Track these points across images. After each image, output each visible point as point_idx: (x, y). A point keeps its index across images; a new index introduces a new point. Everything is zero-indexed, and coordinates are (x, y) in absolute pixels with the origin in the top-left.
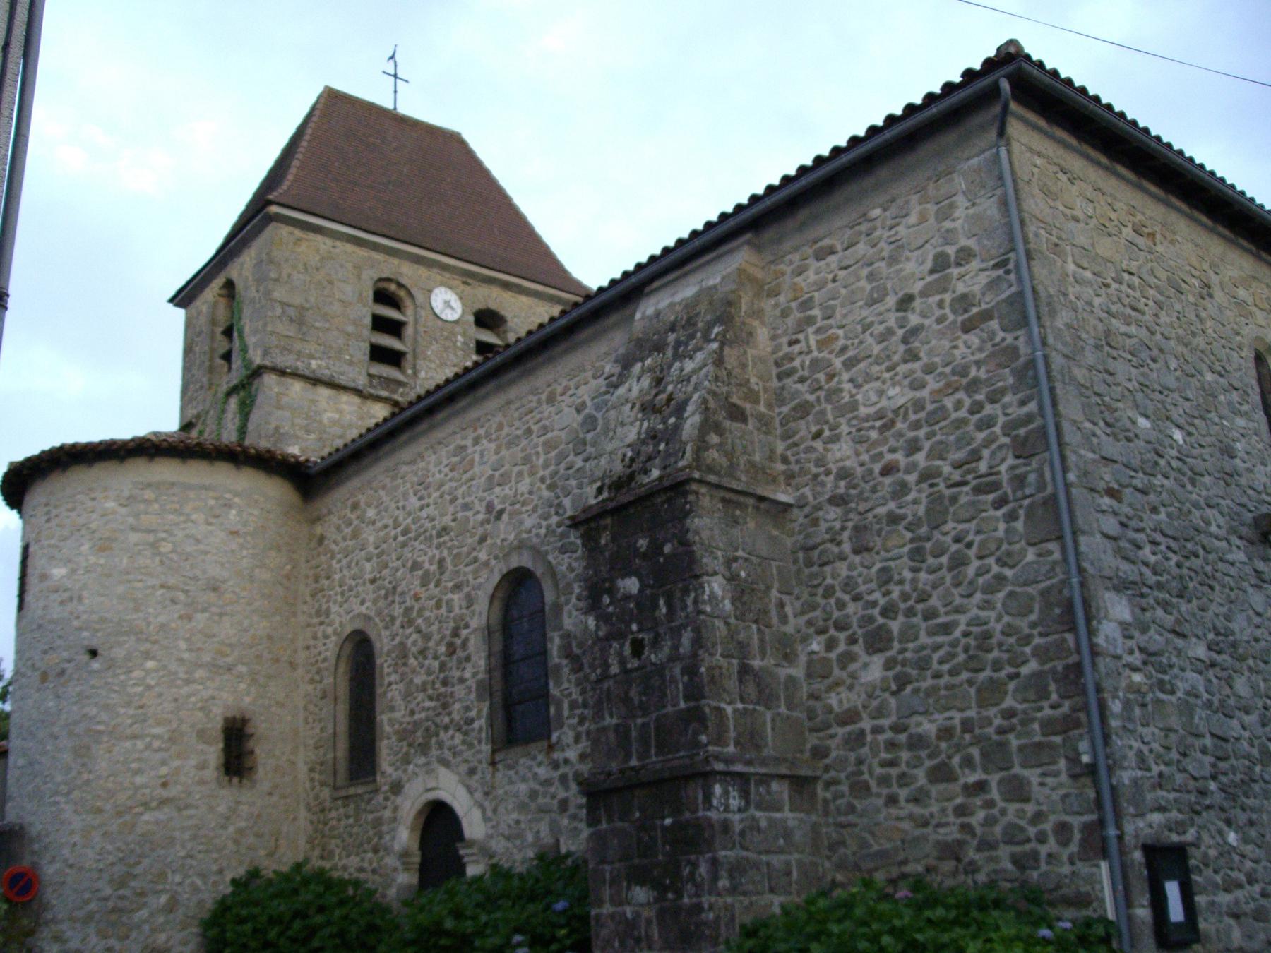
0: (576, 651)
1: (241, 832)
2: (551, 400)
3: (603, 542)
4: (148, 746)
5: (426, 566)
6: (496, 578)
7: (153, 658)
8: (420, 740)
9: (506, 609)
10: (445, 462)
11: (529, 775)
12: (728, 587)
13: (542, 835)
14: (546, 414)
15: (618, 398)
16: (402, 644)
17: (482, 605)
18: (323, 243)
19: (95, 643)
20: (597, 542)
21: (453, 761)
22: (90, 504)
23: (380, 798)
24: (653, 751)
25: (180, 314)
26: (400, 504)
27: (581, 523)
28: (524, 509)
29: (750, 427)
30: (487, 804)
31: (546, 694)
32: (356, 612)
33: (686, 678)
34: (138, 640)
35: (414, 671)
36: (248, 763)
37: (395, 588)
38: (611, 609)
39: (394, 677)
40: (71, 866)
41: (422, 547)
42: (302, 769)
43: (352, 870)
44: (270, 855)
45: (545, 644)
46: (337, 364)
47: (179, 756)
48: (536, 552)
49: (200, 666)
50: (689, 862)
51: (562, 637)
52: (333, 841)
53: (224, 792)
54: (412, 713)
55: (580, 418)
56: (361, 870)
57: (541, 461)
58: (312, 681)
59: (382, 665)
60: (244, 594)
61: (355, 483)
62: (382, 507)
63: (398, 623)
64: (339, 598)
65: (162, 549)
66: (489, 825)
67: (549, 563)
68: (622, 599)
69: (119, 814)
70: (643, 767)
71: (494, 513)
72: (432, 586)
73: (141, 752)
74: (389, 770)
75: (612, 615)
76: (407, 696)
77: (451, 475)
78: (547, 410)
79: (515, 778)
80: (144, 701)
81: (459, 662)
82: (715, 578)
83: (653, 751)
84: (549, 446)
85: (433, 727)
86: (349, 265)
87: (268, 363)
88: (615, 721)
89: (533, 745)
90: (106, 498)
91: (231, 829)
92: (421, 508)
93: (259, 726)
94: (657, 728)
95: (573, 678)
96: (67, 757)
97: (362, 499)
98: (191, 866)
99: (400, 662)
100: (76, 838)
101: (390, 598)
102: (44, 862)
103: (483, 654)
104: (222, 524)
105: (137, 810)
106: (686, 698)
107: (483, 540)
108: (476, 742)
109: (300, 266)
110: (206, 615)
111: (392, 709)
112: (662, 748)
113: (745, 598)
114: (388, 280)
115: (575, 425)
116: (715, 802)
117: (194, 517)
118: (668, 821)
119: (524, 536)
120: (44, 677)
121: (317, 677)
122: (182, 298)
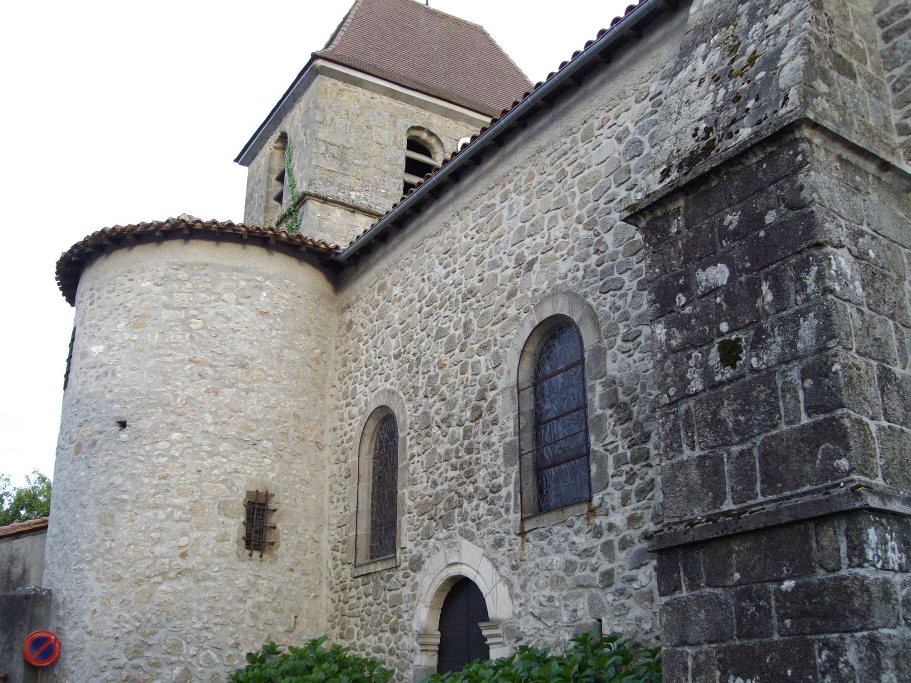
0: (622, 398)
1: (259, 606)
2: (586, 138)
3: (674, 230)
4: (169, 517)
5: (452, 331)
6: (528, 330)
7: (179, 430)
8: (443, 513)
9: (538, 366)
10: (472, 225)
11: (565, 545)
12: (856, 266)
13: (580, 613)
14: (582, 151)
15: (679, 82)
16: (425, 413)
17: (511, 361)
18: (364, 95)
19: (124, 416)
20: (665, 232)
21: (477, 533)
22: (128, 284)
23: (400, 574)
24: (758, 487)
25: (244, 171)
26: (425, 277)
27: (641, 212)
28: (558, 255)
29: (859, 85)
30: (515, 579)
31: (585, 453)
32: (381, 389)
33: (809, 383)
34: (166, 412)
35: (437, 441)
36: (271, 538)
37: (418, 359)
38: (688, 310)
39: (416, 449)
40: (90, 633)
41: (448, 313)
42: (326, 547)
43: (370, 650)
44: (289, 631)
45: (585, 397)
46: (374, 196)
47: (199, 528)
48: (572, 295)
49: (225, 439)
50: (826, 644)
51: (604, 385)
52: (352, 620)
53: (244, 565)
54: (435, 484)
55: (622, 147)
56: (379, 650)
57: (577, 200)
58: (338, 461)
59: (405, 438)
60: (273, 372)
61: (383, 264)
62: (407, 283)
63: (421, 393)
64: (365, 378)
65: (192, 326)
66: (516, 603)
67: (590, 306)
68: (704, 296)
69: (138, 583)
70: (743, 511)
71: (524, 265)
72: (457, 351)
73: (162, 521)
74: (410, 546)
75: (689, 317)
76: (429, 468)
77: (477, 236)
78: (582, 147)
79: (547, 548)
80: (168, 471)
81: (485, 426)
82: (839, 251)
83: (758, 487)
84: (585, 185)
85: (456, 497)
86: (386, 114)
87: (311, 191)
88: (698, 452)
89: (570, 510)
90: (143, 278)
91: (250, 603)
92: (447, 276)
93: (282, 502)
94: (764, 456)
95: (619, 429)
96: (93, 525)
97: (389, 280)
98: (207, 639)
99: (423, 433)
100: (96, 605)
101: (415, 370)
102: (66, 628)
103: (512, 415)
104: (252, 305)
105: (155, 579)
106: (809, 411)
107: (512, 294)
108: (502, 511)
109: (343, 113)
110: (234, 390)
111: (414, 482)
112: (771, 482)
113: (877, 285)
114: (420, 128)
115: (616, 155)
116: (870, 554)
117: (225, 296)
118: (788, 585)
119: (559, 282)
120: (78, 449)
121: (342, 457)
122: (246, 157)
